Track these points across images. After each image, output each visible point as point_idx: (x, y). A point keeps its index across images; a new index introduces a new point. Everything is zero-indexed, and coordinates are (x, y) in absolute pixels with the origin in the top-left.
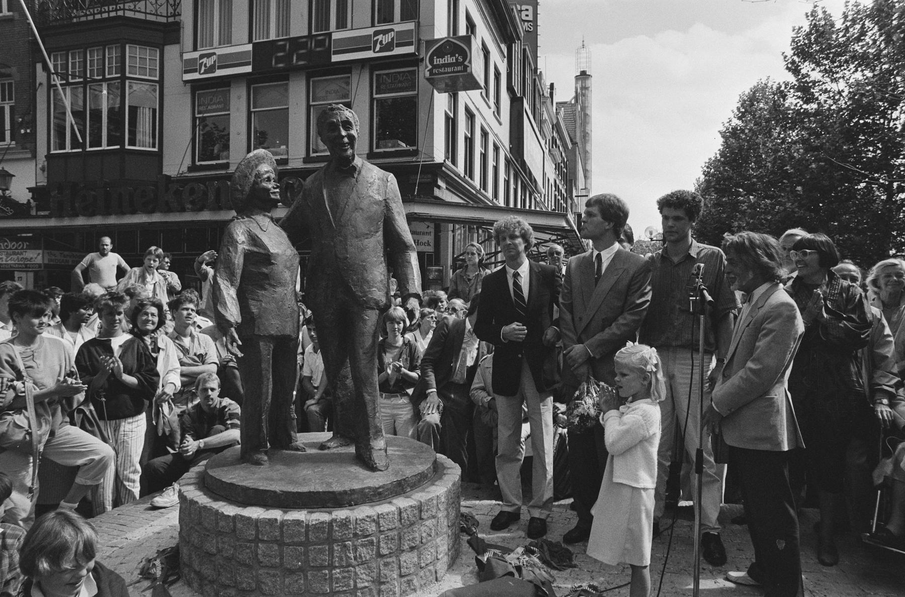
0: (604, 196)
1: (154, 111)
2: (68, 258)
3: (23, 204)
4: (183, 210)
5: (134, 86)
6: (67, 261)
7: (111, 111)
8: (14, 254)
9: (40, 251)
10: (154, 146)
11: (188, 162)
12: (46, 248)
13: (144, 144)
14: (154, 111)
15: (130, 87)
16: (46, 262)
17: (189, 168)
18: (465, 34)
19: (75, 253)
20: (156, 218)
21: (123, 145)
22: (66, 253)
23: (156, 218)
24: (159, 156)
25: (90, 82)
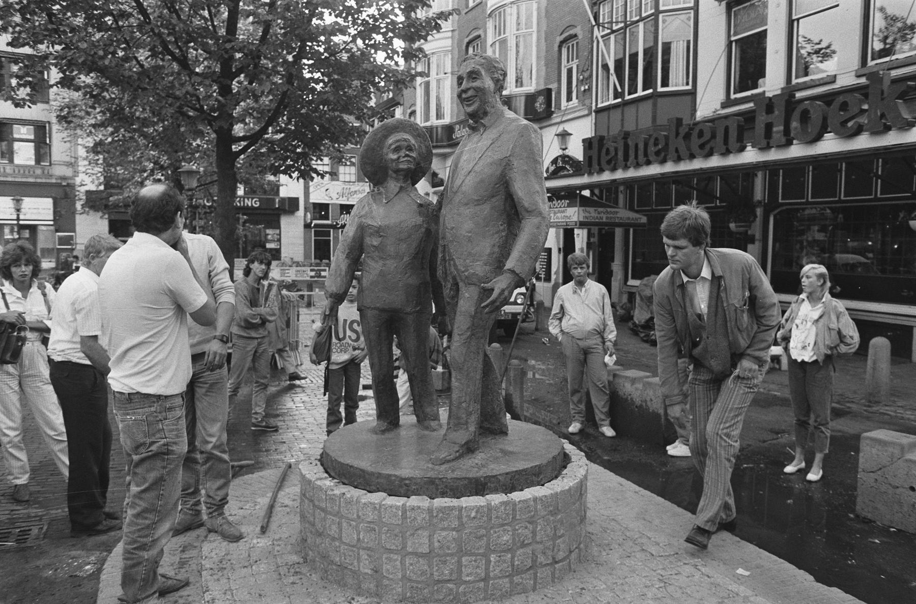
0: (904, 134)
1: (688, 42)
2: (602, 215)
3: (141, 230)
4: (692, 157)
5: (667, 18)
6: (602, 218)
7: (646, 51)
8: (559, 212)
9: (576, 209)
10: (687, 84)
11: (722, 97)
12: (580, 206)
13: (678, 83)
14: (688, 42)
15: (664, 21)
16: (581, 219)
17: (722, 104)
18: (48, 203)
19: (609, 210)
20: (669, 168)
21: (655, 89)
22: (600, 209)
23: (669, 168)
24: (692, 94)
25: (630, 25)
